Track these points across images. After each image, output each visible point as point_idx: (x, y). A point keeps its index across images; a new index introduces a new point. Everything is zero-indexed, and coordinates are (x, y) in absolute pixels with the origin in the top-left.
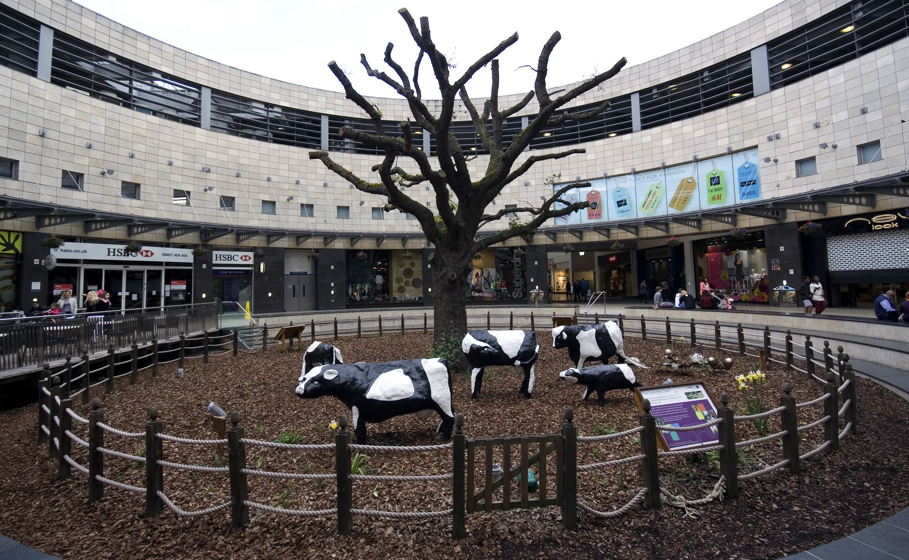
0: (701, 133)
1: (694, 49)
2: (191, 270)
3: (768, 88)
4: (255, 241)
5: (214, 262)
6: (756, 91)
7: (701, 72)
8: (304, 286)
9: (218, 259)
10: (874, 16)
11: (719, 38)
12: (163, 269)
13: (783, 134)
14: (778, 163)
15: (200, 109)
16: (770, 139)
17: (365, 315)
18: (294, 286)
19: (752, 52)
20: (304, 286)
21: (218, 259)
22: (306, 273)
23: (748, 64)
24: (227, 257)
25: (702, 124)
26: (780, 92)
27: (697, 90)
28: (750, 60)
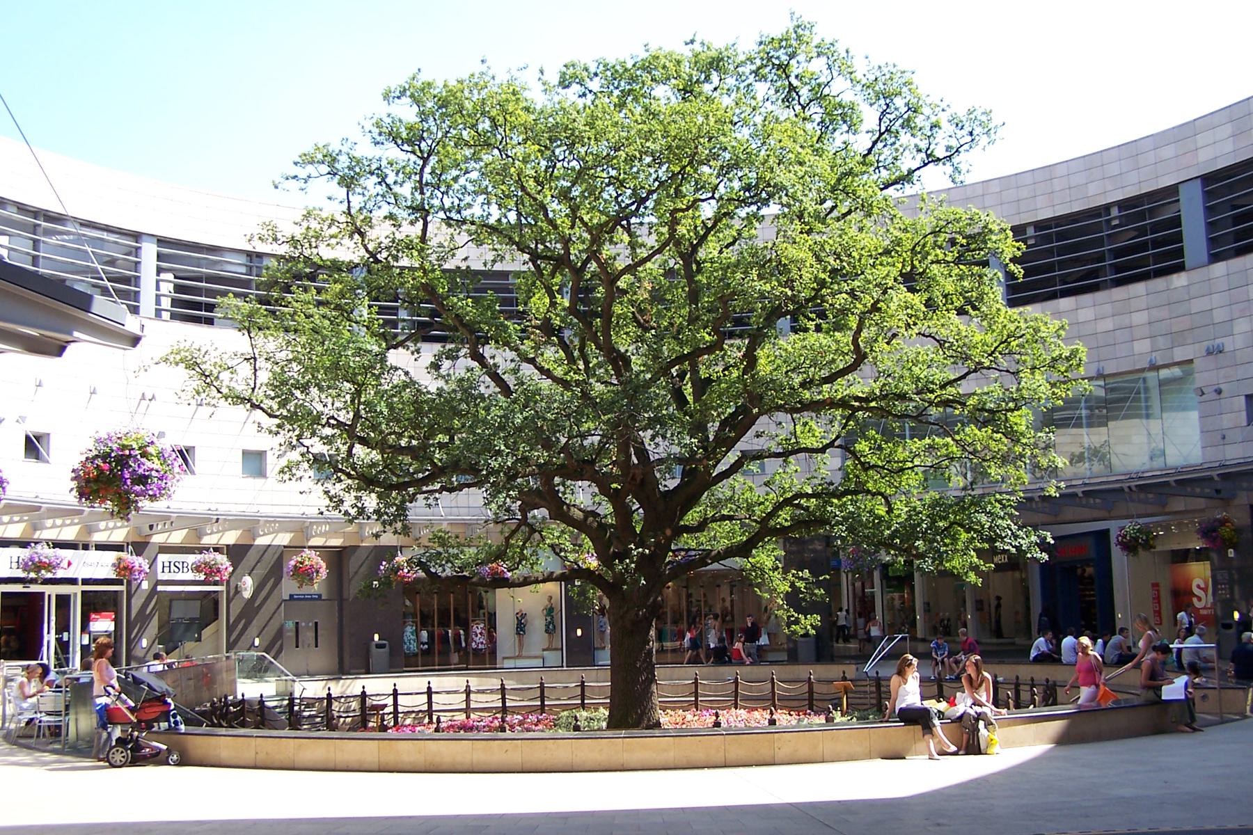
0: (1107, 325)
1: (1092, 162)
2: (122, 591)
3: (1205, 258)
4: (413, 715)
5: (161, 577)
6: (1188, 259)
7: (1107, 208)
8: (316, 623)
9: (166, 570)
10: (1235, 203)
11: (1131, 151)
12: (77, 590)
13: (1228, 344)
14: (1222, 395)
15: (137, 293)
16: (1209, 353)
17: (440, 682)
18: (297, 623)
19: (1180, 186)
20: (316, 623)
21: (166, 570)
22: (320, 596)
23: (1173, 208)
24: (180, 567)
25: (1108, 308)
26: (1220, 268)
27: (1099, 242)
28: (1178, 200)
